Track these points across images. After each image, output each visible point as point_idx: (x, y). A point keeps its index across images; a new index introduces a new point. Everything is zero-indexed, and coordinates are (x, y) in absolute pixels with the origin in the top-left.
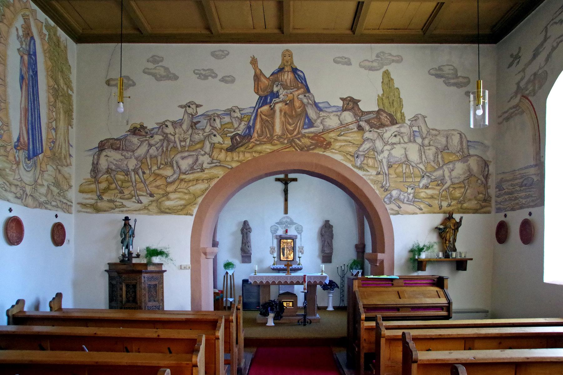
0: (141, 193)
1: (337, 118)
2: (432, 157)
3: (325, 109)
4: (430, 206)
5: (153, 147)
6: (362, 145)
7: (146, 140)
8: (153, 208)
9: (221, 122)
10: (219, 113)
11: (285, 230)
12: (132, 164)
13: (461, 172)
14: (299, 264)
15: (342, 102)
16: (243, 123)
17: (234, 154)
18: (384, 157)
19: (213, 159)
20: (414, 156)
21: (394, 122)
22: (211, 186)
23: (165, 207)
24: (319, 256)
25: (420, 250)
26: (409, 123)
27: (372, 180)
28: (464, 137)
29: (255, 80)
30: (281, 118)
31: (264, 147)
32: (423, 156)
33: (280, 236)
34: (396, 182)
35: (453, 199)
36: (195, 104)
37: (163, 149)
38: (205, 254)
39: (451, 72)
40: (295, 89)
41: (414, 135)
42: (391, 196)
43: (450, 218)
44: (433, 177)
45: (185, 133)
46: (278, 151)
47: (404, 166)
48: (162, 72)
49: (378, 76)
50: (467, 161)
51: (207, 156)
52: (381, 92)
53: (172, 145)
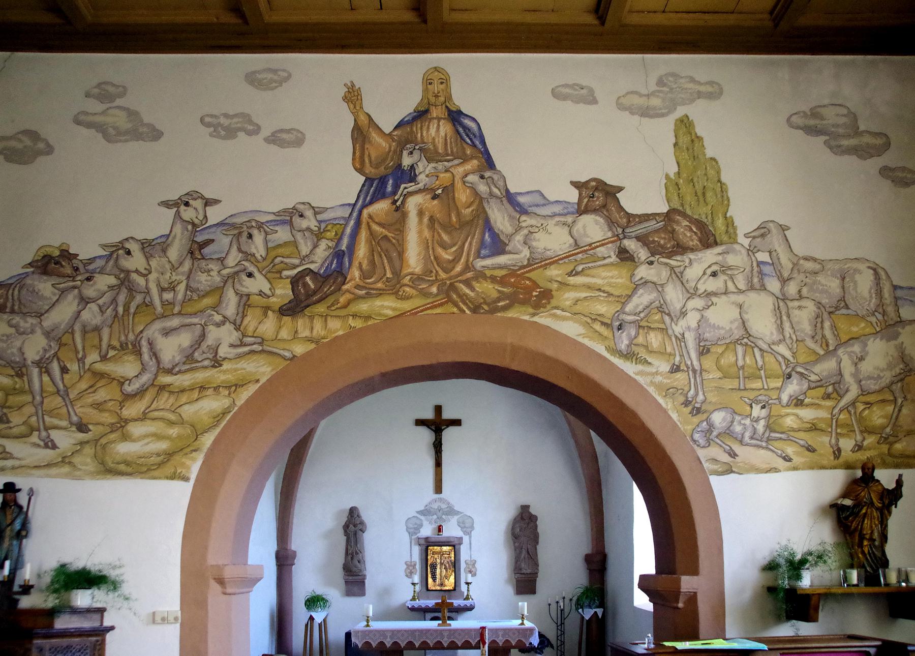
0: (56, 422)
1: (566, 229)
2: (807, 327)
3: (534, 209)
4: (811, 449)
5: (93, 306)
6: (630, 297)
7: (75, 287)
8: (86, 460)
9: (266, 241)
10: (263, 219)
11: (436, 526)
12: (35, 347)
13: (881, 362)
14: (467, 598)
15: (575, 193)
16: (323, 244)
17: (300, 322)
18: (689, 328)
19: (244, 336)
20: (763, 324)
21: (708, 240)
22: (239, 403)
23: (118, 458)
24: (509, 581)
25: (796, 567)
26: (746, 242)
27: (659, 387)
28: (883, 276)
29: (354, 140)
30: (420, 232)
31: (378, 302)
32: (787, 326)
33: (427, 539)
34: (719, 389)
35: (868, 431)
36: (202, 197)
37: (115, 310)
38: (221, 582)
39: (843, 120)
40: (456, 162)
41: (761, 273)
42: (711, 426)
43: (868, 478)
44: (813, 378)
45: (174, 268)
46: (414, 313)
47: (740, 350)
48: (121, 120)
49: (663, 131)
50: (896, 336)
51: (228, 326)
52: (673, 169)
53: (139, 299)
